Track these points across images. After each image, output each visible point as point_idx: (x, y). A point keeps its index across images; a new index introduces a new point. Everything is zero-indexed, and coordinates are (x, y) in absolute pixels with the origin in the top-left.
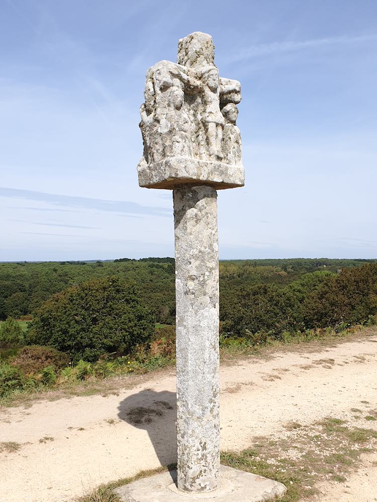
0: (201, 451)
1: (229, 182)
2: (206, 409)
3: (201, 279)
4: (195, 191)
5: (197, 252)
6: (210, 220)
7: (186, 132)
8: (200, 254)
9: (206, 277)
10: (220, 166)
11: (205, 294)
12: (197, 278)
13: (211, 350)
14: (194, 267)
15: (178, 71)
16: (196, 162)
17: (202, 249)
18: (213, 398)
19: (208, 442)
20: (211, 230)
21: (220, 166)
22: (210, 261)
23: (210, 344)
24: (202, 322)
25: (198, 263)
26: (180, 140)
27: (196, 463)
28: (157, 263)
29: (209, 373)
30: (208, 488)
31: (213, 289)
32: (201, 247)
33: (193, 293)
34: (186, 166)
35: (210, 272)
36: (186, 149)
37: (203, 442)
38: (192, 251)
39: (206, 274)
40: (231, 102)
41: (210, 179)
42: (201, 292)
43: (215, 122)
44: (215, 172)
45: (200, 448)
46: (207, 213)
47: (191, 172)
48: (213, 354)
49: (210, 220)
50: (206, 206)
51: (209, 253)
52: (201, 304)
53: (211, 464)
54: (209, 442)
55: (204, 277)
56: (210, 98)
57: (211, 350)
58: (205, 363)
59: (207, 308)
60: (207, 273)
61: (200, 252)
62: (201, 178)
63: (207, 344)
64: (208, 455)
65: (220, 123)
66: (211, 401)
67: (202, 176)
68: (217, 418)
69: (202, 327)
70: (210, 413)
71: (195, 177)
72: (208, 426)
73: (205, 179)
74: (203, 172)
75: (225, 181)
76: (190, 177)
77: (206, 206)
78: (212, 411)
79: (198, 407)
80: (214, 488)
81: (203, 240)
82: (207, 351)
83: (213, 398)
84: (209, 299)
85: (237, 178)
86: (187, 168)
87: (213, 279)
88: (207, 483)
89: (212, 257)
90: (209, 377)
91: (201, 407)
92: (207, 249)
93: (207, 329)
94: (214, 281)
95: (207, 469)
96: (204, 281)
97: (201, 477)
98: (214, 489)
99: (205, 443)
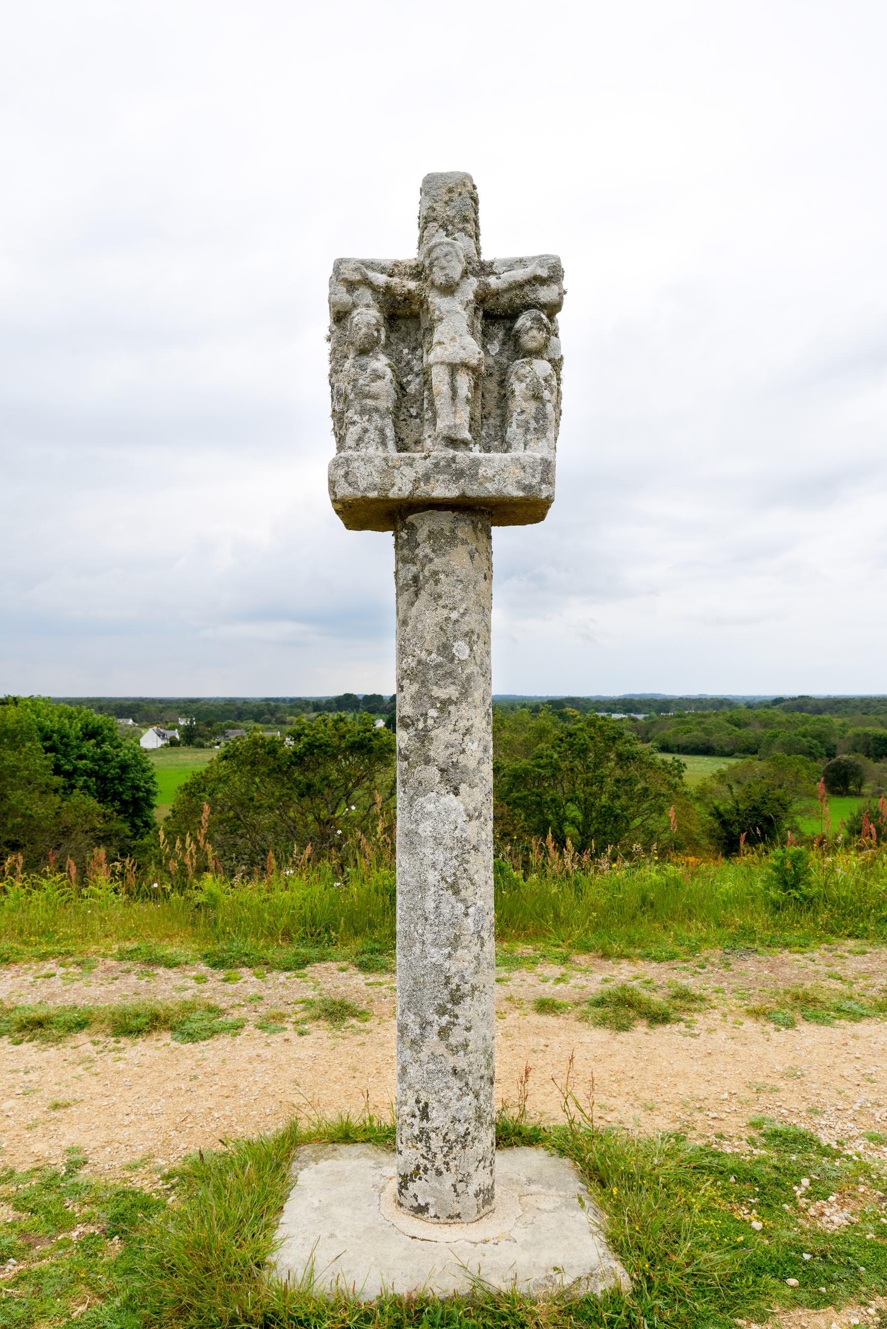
0: (418, 1119)
1: (483, 495)
2: (429, 1027)
3: (421, 725)
4: (413, 524)
5: (413, 664)
6: (442, 588)
7: (377, 399)
8: (420, 667)
9: (430, 722)
10: (453, 459)
11: (427, 761)
12: (413, 724)
13: (441, 892)
14: (408, 697)
15: (361, 274)
16: (377, 461)
17: (424, 655)
18: (449, 1006)
19: (433, 1104)
20: (445, 612)
21: (453, 459)
22: (442, 683)
23: (439, 878)
24: (422, 825)
25: (415, 687)
26: (356, 418)
27: (410, 1144)
28: (604, 714)
29: (435, 943)
30: (432, 1212)
31: (451, 750)
32: (422, 651)
33: (406, 758)
34: (347, 473)
35: (441, 710)
36: (373, 435)
37: (423, 1102)
38: (405, 660)
39: (430, 714)
40: (527, 307)
41: (418, 493)
42: (420, 756)
43: (442, 363)
44: (437, 477)
45: (418, 1113)
46: (436, 573)
47: (363, 484)
48: (448, 902)
49: (442, 588)
50: (432, 555)
51: (439, 666)
52: (420, 782)
53: (440, 1156)
54: (436, 1105)
55: (425, 721)
56: (437, 313)
57: (441, 892)
58: (426, 919)
59: (433, 794)
60: (433, 713)
61: (419, 662)
62: (393, 494)
63: (432, 877)
64: (433, 1135)
65: (458, 361)
66: (442, 1011)
67: (396, 488)
68: (462, 1053)
69: (421, 837)
70: (436, 1038)
71: (373, 494)
72: (432, 1067)
73: (405, 493)
74: (398, 481)
75: (469, 493)
76: (359, 495)
77: (432, 555)
78: (444, 1033)
79: (413, 1017)
80: (450, 1217)
81: (425, 634)
82: (430, 893)
83: (449, 1006)
84: (439, 774)
85: (509, 481)
86: (350, 476)
87: (451, 727)
88: (431, 1200)
89: (449, 674)
90: (436, 955)
91: (419, 1020)
92: (434, 656)
93: (431, 843)
94: (455, 731)
95: (429, 1166)
96: (426, 730)
97: (417, 1179)
98: (450, 1221)
99: (426, 1105)
